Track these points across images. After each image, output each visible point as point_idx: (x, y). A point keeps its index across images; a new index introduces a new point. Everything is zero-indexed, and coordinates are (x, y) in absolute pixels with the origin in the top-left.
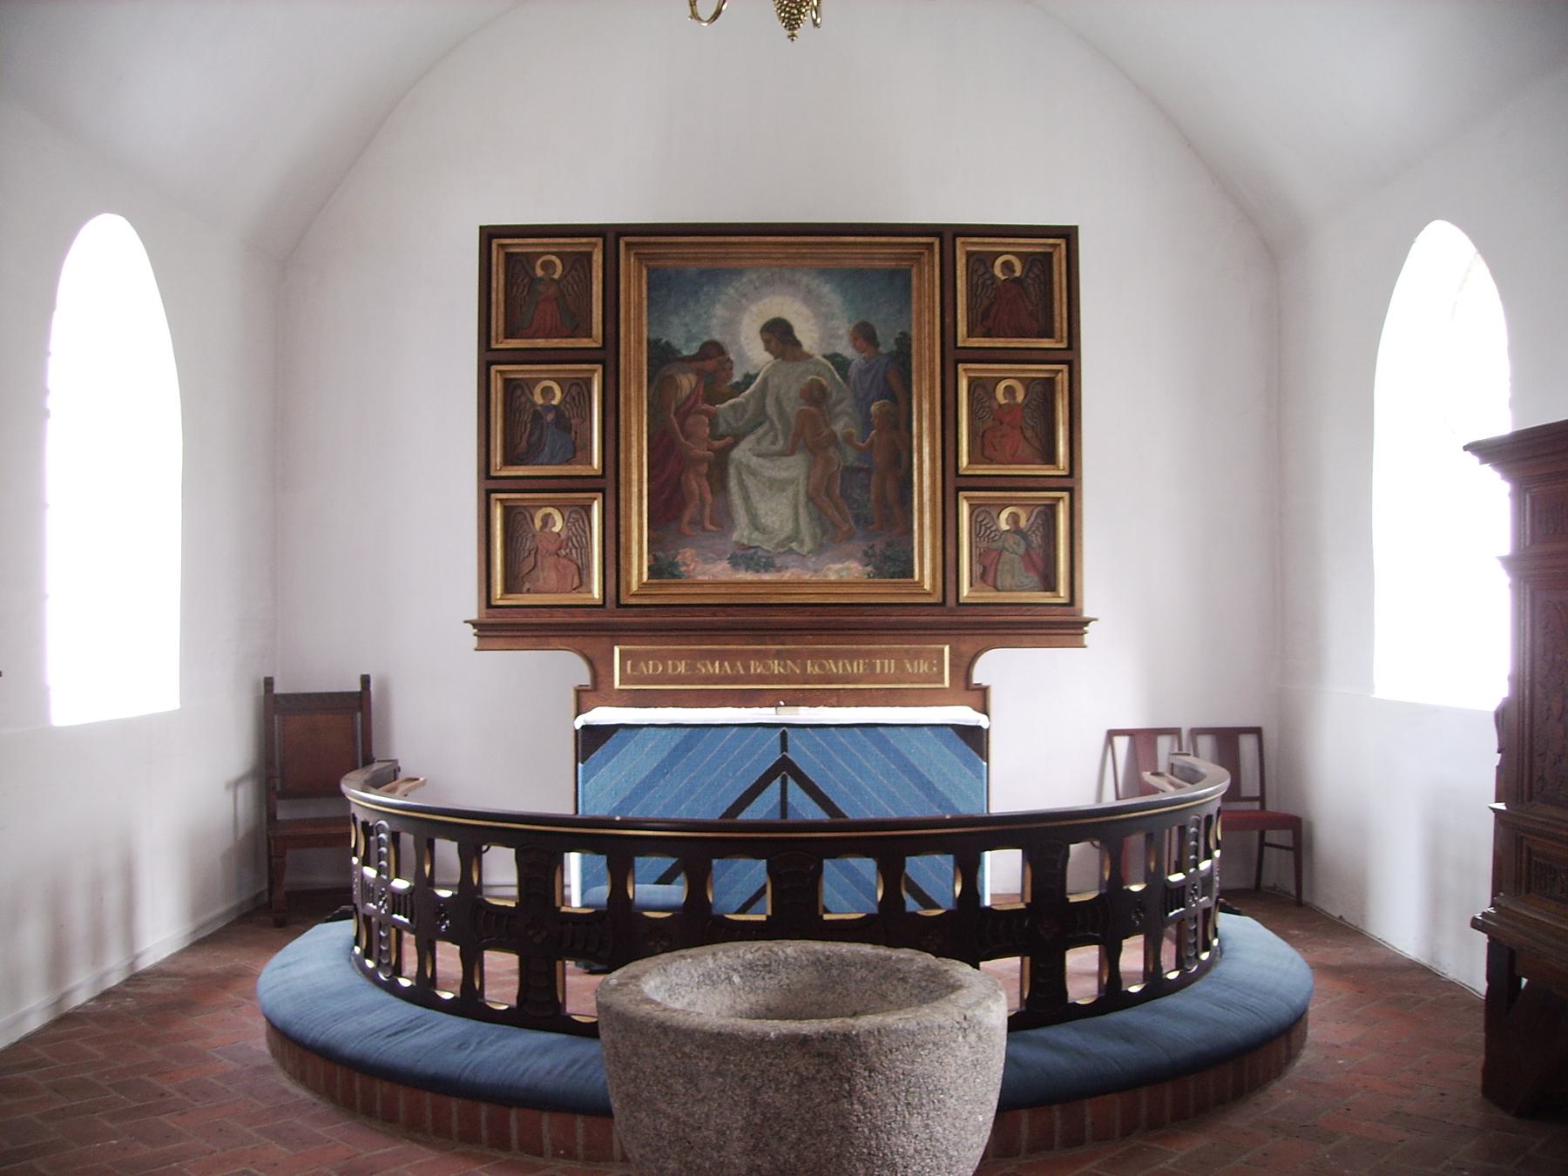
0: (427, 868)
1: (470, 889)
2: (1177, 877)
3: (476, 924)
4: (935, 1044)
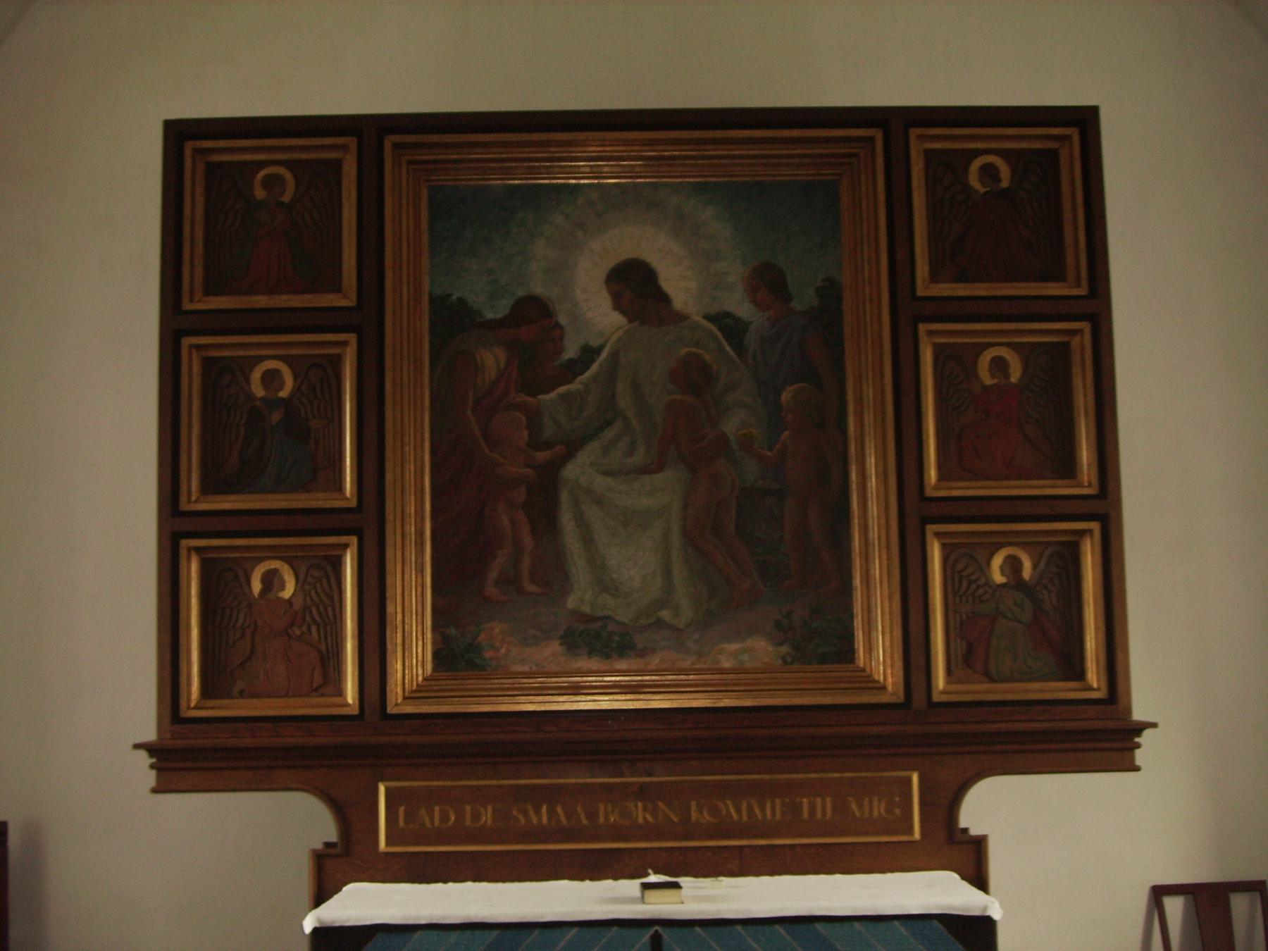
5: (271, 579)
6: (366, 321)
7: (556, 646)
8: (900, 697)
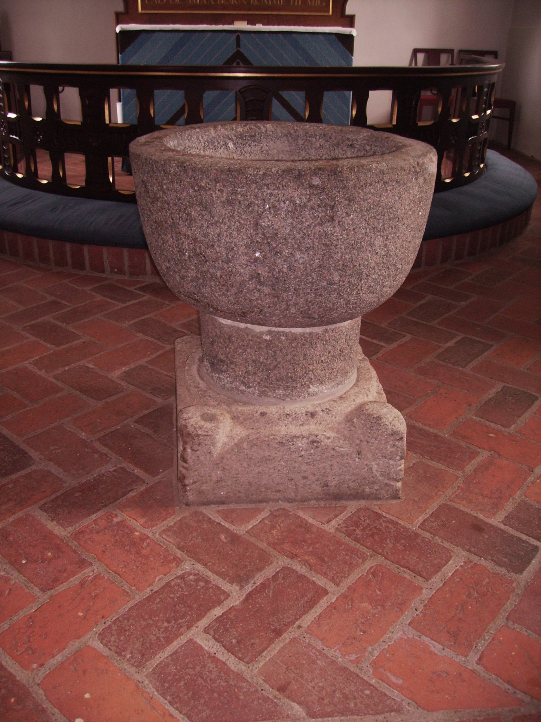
0: (26, 103)
1: (52, 116)
2: (475, 117)
3: (58, 137)
4: (397, 182)
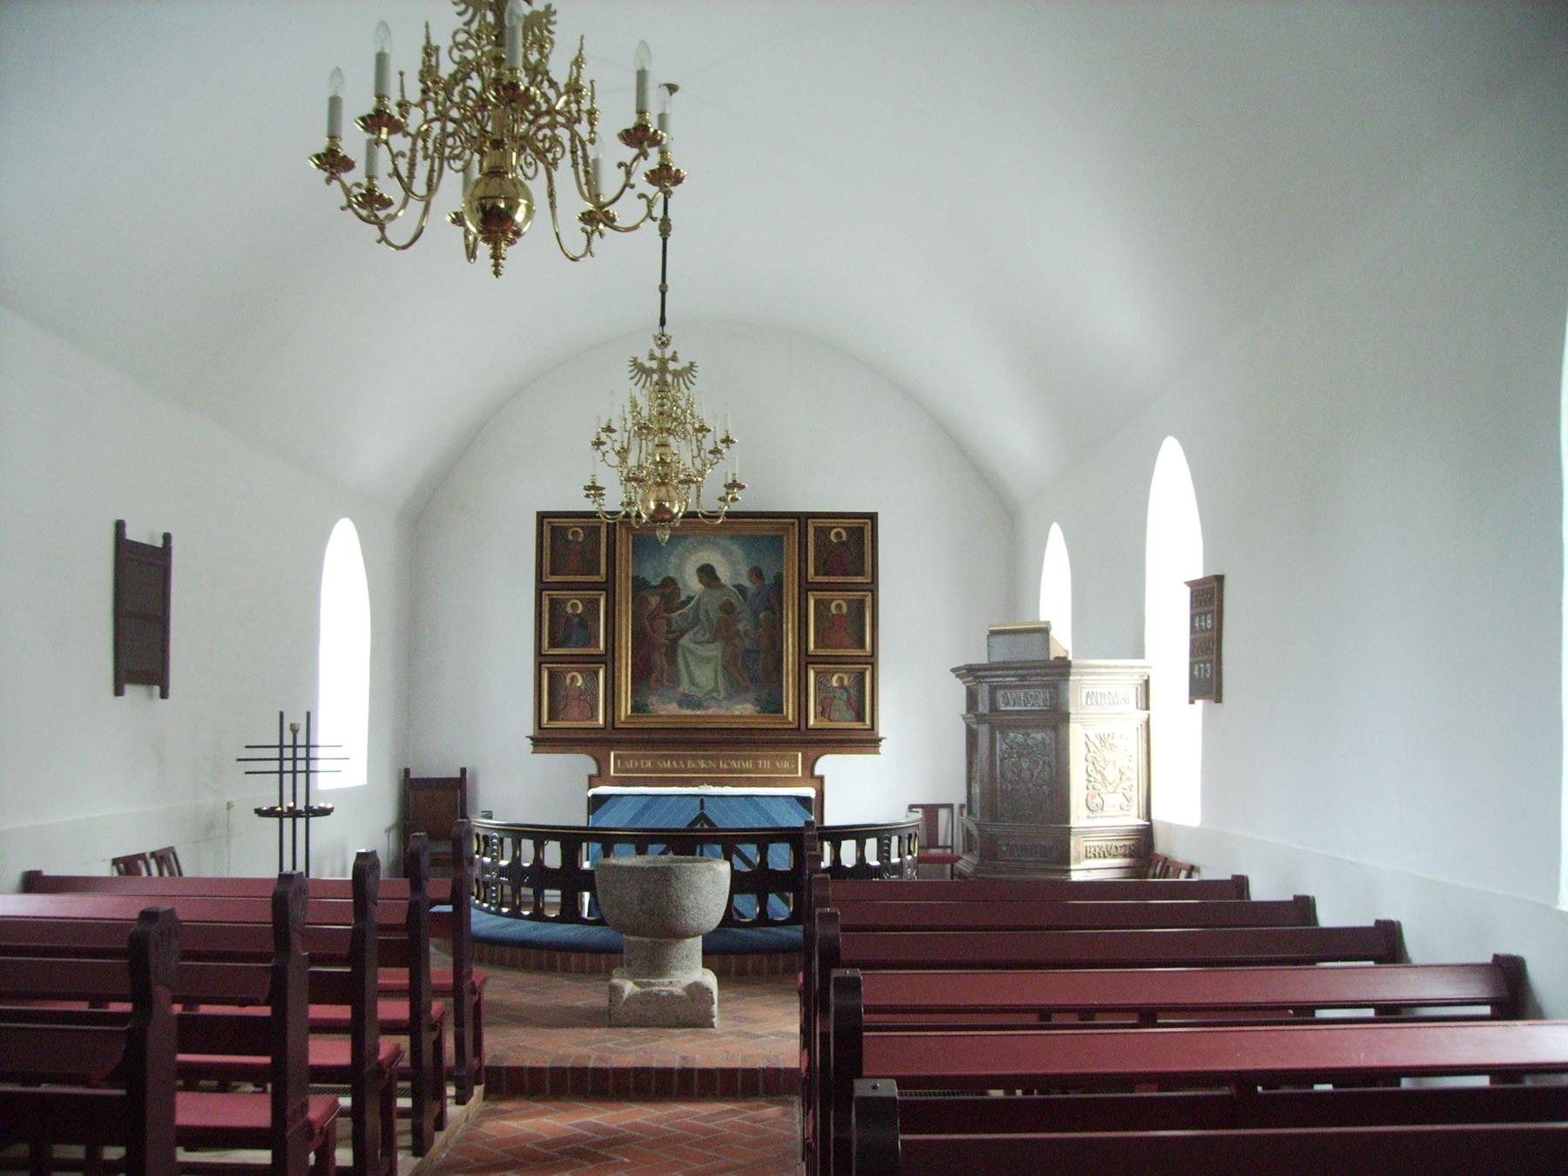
1: (538, 861)
5: (573, 678)
6: (609, 586)
7: (674, 705)
8: (795, 725)
